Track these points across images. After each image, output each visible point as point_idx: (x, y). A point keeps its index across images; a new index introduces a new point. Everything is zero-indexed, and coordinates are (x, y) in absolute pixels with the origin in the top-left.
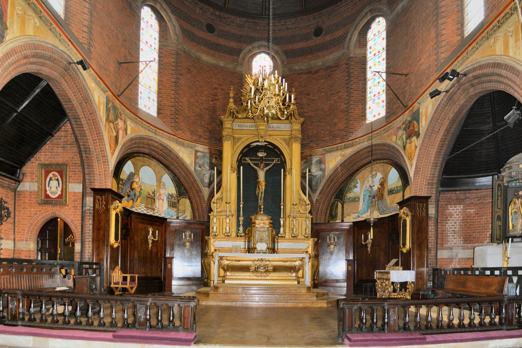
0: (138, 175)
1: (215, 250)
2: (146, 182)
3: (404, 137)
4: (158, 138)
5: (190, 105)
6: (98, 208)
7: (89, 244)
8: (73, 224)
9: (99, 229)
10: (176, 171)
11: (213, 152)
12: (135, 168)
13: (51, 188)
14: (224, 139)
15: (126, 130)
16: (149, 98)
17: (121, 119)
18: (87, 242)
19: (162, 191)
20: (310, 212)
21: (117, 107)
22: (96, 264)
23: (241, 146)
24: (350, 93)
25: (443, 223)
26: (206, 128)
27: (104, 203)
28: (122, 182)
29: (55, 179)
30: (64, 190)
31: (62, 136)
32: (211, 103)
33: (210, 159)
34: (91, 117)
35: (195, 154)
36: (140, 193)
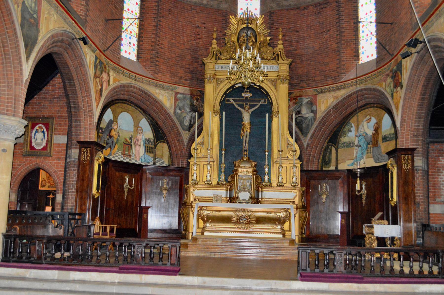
0: (117, 122)
1: (195, 200)
2: (124, 128)
3: (392, 85)
4: (138, 84)
5: (171, 47)
6: (83, 160)
7: (72, 195)
8: (55, 174)
9: (83, 180)
10: (154, 115)
11: (195, 93)
12: (114, 116)
13: (36, 140)
14: (206, 81)
15: (109, 81)
16: (130, 43)
17: (105, 72)
18: (70, 192)
19: (139, 137)
20: (300, 158)
21: (103, 62)
22: (78, 214)
23: (225, 87)
24: (341, 32)
25: (435, 175)
26: (187, 68)
27: (89, 155)
28: (102, 131)
29: (41, 131)
30: (49, 141)
31: (49, 90)
32: (193, 42)
33: (191, 101)
34: (83, 78)
35: (175, 97)
36: (118, 140)
